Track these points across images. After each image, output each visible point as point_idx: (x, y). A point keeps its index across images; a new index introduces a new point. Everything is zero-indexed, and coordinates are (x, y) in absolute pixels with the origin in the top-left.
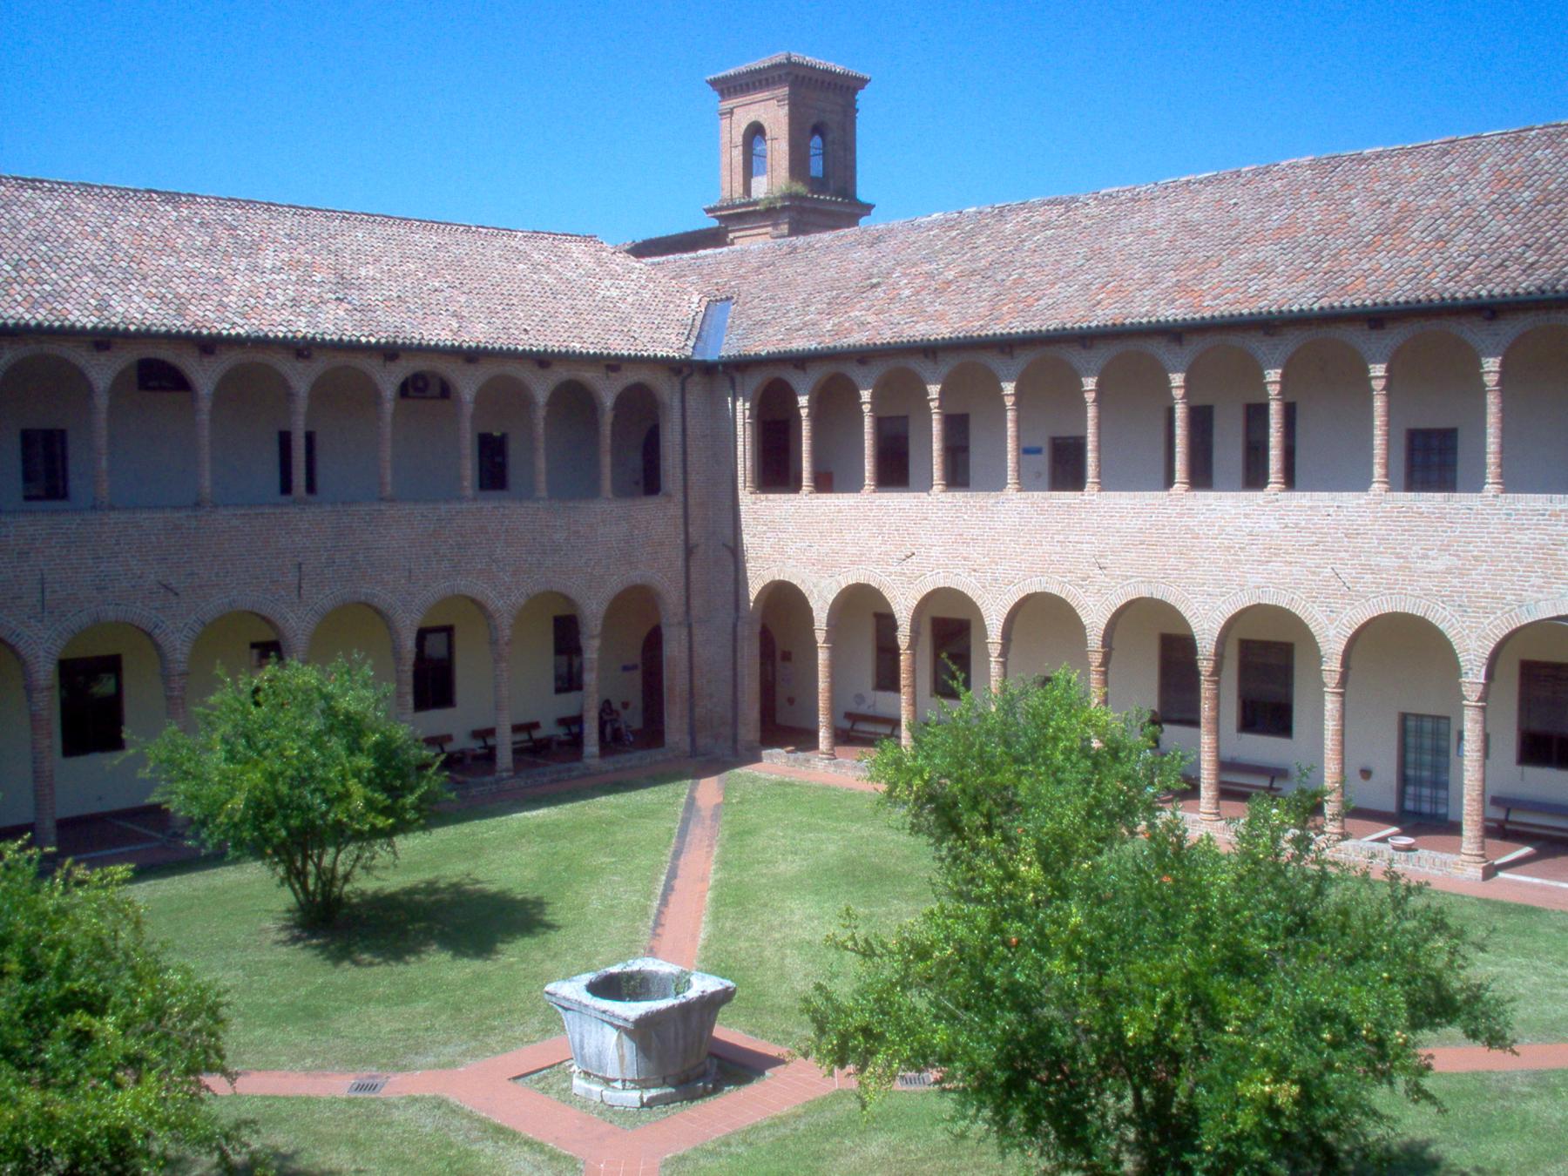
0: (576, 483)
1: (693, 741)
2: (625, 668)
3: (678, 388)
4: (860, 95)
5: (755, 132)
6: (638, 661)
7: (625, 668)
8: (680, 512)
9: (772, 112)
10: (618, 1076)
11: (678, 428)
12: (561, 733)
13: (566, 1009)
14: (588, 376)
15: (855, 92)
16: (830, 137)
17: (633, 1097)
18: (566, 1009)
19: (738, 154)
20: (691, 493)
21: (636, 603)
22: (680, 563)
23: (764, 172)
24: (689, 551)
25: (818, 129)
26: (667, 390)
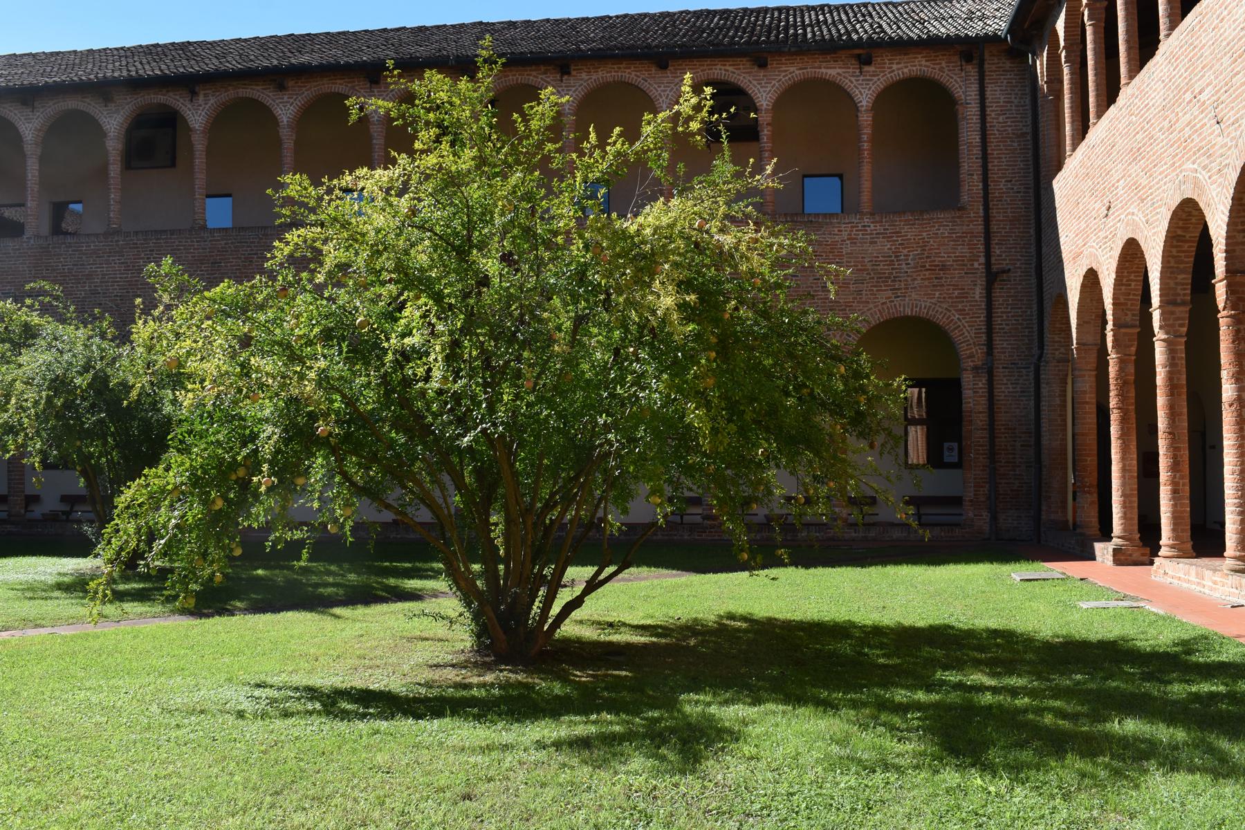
1: (994, 518)
11: (975, 119)
14: (832, 71)
22: (978, 293)
24: (992, 277)
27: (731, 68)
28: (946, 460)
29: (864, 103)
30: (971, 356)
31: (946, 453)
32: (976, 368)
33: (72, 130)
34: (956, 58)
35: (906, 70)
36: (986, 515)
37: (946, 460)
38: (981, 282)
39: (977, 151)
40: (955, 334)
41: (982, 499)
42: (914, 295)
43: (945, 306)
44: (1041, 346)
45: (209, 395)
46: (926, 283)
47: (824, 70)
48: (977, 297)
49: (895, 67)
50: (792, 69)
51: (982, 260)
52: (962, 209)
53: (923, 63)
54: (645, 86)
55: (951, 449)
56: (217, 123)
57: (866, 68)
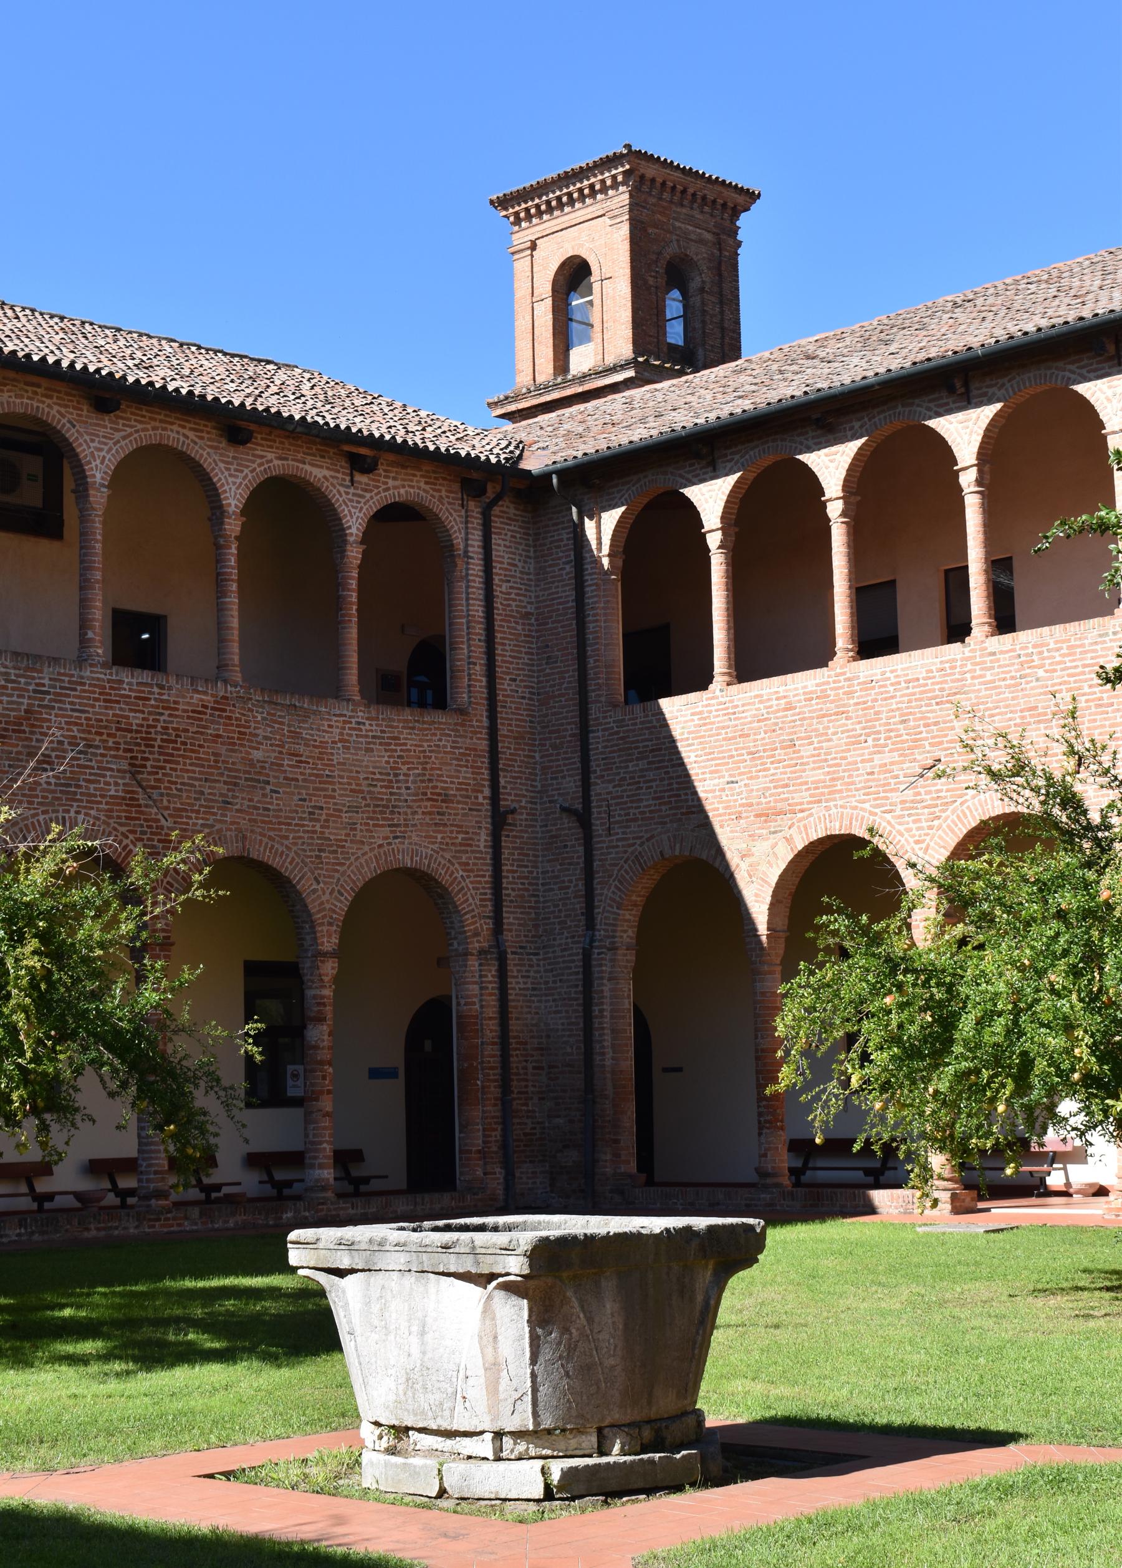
0: (298, 669)
1: (509, 1175)
2: (375, 1074)
3: (476, 522)
4: (746, 222)
5: (574, 275)
6: (396, 1058)
7: (375, 1074)
8: (484, 745)
9: (603, 234)
10: (486, 1425)
11: (477, 582)
12: (250, 1183)
13: (340, 1273)
14: (321, 473)
15: (736, 213)
16: (694, 284)
17: (525, 1478)
18: (340, 1273)
19: (545, 313)
20: (502, 714)
21: (405, 899)
22: (483, 839)
23: (588, 339)
24: (499, 819)
25: (677, 274)
26: (459, 523)
27: (191, 434)
28: (291, 1092)
29: (354, 530)
30: (476, 934)
31: (290, 1083)
32: (482, 952)
33: (162, 474)
34: (456, 486)
35: (402, 491)
36: (499, 1172)
37: (291, 1092)
38: (487, 824)
39: (479, 629)
40: (459, 899)
41: (495, 1149)
42: (415, 839)
43: (448, 856)
44: (590, 925)
45: (1093, 1059)
46: (428, 818)
47: (307, 467)
48: (482, 844)
49: (391, 483)
50: (270, 456)
51: (487, 792)
52: (462, 712)
53: (422, 485)
54: (71, 434)
55: (295, 1076)
56: (126, 472)
57: (358, 477)
